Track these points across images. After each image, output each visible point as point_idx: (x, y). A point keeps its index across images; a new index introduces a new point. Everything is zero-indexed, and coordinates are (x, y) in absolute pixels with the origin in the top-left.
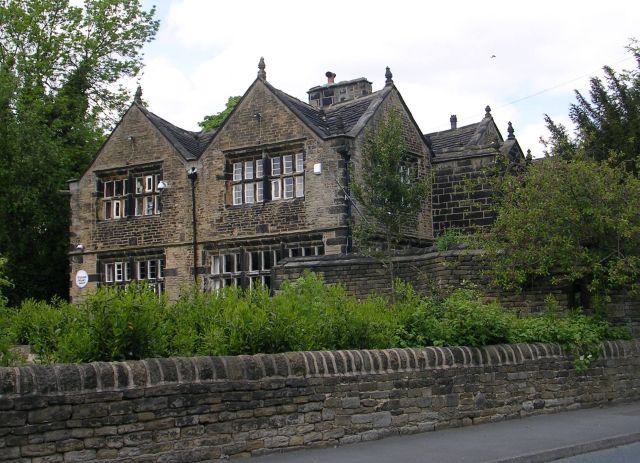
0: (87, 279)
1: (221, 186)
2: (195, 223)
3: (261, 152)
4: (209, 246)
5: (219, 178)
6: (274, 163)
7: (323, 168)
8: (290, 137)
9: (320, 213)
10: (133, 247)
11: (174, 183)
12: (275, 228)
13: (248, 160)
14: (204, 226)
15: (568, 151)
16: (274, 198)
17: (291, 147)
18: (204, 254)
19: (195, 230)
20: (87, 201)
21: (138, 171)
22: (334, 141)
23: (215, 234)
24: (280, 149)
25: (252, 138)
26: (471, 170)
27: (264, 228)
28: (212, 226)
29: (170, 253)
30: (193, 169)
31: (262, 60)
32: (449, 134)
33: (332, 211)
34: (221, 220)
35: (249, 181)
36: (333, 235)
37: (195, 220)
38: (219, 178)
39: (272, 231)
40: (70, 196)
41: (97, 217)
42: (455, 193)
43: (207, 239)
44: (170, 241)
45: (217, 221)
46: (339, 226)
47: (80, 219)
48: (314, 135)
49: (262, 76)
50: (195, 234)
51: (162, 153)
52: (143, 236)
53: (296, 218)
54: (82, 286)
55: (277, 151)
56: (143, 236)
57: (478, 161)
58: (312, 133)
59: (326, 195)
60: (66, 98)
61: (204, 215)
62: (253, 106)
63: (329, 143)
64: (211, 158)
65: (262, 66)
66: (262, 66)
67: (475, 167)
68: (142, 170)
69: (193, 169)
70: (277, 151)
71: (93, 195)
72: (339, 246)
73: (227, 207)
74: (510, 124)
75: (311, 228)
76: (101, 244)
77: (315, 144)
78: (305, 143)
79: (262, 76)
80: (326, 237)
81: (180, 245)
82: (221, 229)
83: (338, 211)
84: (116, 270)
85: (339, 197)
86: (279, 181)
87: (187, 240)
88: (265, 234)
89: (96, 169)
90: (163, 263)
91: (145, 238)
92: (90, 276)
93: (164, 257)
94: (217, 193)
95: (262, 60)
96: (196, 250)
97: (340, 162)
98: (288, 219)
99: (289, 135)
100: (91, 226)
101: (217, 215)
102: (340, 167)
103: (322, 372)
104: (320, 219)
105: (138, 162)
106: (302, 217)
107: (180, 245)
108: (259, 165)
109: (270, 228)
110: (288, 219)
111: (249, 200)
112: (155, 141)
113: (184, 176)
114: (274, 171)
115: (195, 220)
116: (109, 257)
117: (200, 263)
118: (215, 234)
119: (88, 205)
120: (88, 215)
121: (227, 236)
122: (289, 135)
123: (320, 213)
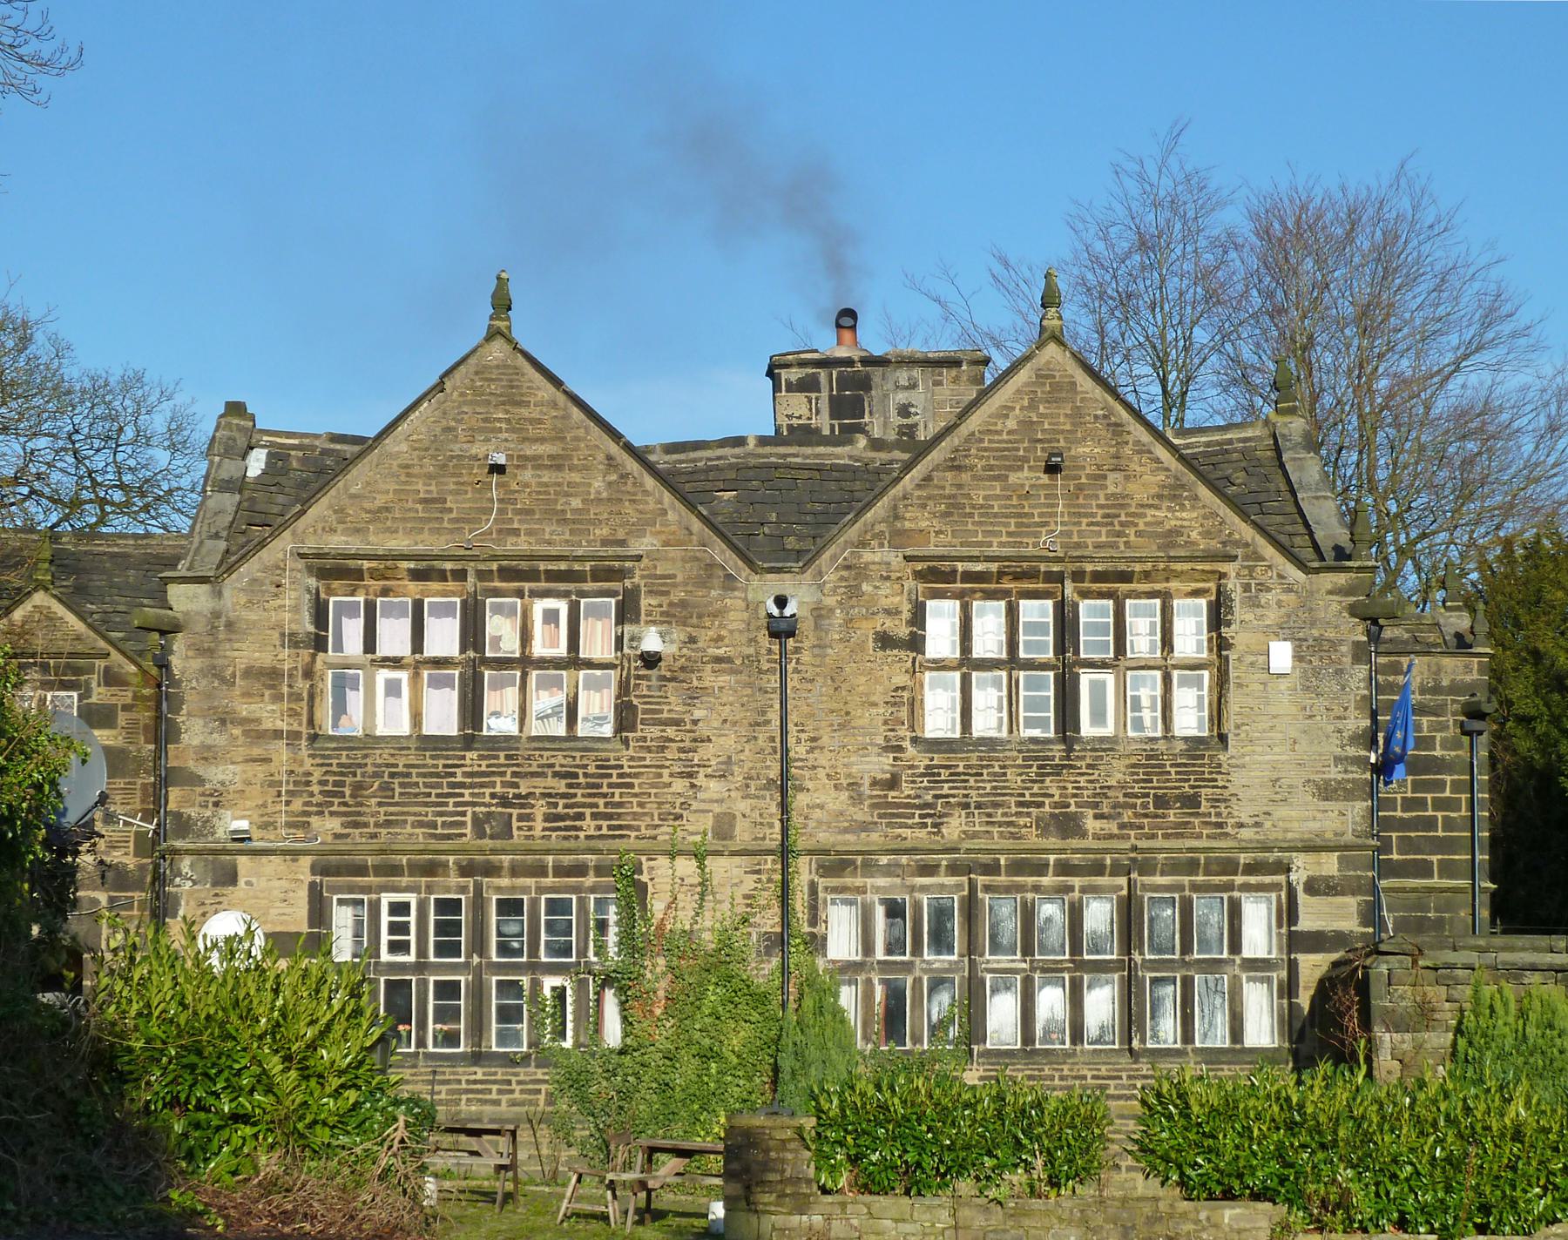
2: (784, 786)
4: (836, 864)
11: (692, 640)
12: (1111, 826)
13: (990, 595)
15: (1490, 557)
18: (813, 888)
19: (784, 807)
21: (507, 574)
23: (865, 827)
25: (1026, 526)
28: (857, 799)
33: (1327, 792)
34: (893, 783)
36: (1330, 865)
37: (785, 775)
40: (136, 855)
43: (824, 838)
46: (1349, 838)
53: (1191, 802)
56: (540, 809)
58: (1261, 541)
60: (85, 1048)
62: (1027, 424)
64: (855, 572)
68: (533, 575)
69: (781, 602)
80: (1303, 868)
82: (890, 812)
83: (1349, 796)
84: (385, 919)
85: (1352, 751)
88: (1075, 843)
89: (311, 545)
91: (548, 818)
97: (1357, 644)
98: (1161, 802)
100: (281, 754)
101: (881, 765)
104: (1281, 812)
105: (522, 545)
108: (1039, 612)
109: (1091, 824)
111: (987, 722)
115: (785, 775)
118: (865, 827)
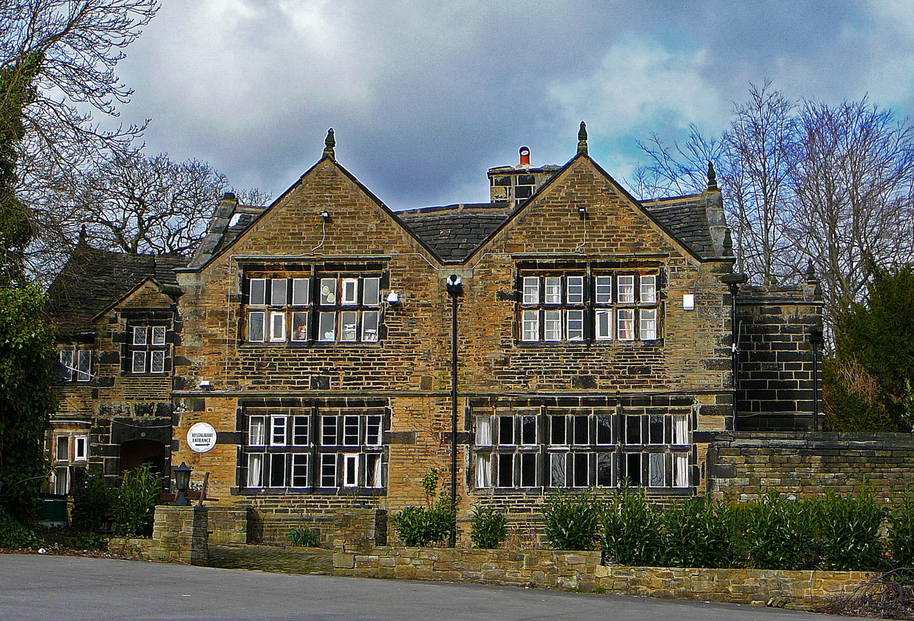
0: (214, 439)
2: (455, 364)
3: (584, 266)
4: (477, 402)
5: (502, 296)
6: (602, 283)
7: (696, 302)
8: (639, 250)
9: (687, 363)
11: (413, 296)
14: (471, 370)
16: (598, 337)
17: (637, 264)
18: (468, 414)
22: (718, 265)
25: (569, 243)
26: (781, 321)
27: (587, 382)
28: (488, 370)
29: (398, 406)
30: (454, 278)
32: (482, 213)
34: (505, 362)
35: (554, 307)
36: (712, 401)
37: (455, 359)
38: (502, 296)
39: (602, 386)
41: (240, 336)
44: (400, 386)
47: (200, 335)
48: (683, 252)
51: (388, 246)
52: (342, 375)
53: (646, 370)
54: (202, 449)
55: (610, 266)
56: (342, 375)
57: (792, 309)
59: (700, 342)
61: (472, 351)
62: (570, 194)
63: (710, 266)
67: (786, 318)
68: (341, 267)
69: (454, 278)
70: (610, 266)
72: (723, 418)
73: (517, 342)
74: (331, 133)
75: (673, 387)
76: (249, 383)
77: (685, 265)
78: (665, 260)
81: (422, 396)
83: (722, 368)
85: (723, 347)
86: (609, 312)
87: (435, 388)
88: (591, 390)
90: (387, 425)
92: (219, 435)
96: (456, 404)
99: (637, 246)
102: (725, 303)
104: (689, 375)
107: (422, 396)
109: (599, 382)
112: (372, 225)
113: (434, 286)
115: (455, 359)
116: (261, 404)
117: (461, 426)
118: (492, 383)
121: (515, 387)
122: (637, 246)
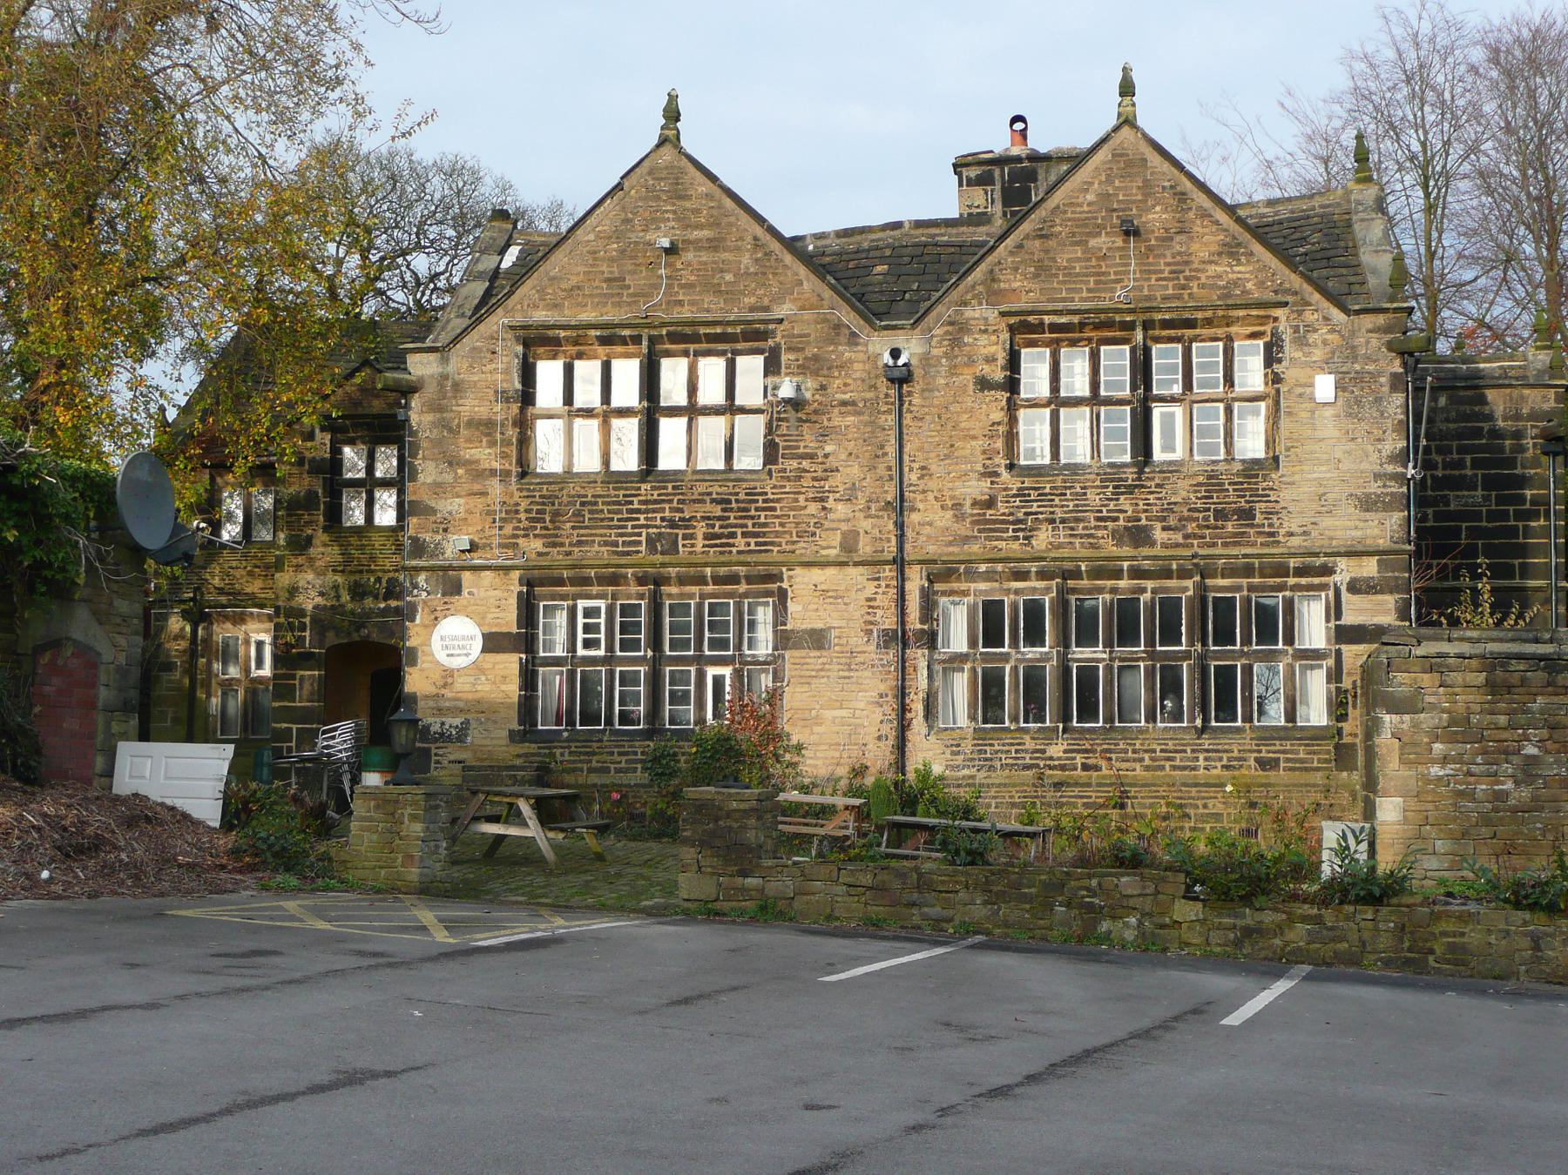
0: (478, 644)
1: (993, 407)
2: (900, 507)
3: (1130, 326)
5: (984, 384)
10: (659, 558)
12: (1179, 538)
20: (483, 412)
22: (1381, 319)
23: (966, 539)
24: (1190, 324)
25: (1103, 284)
28: (960, 517)
31: (672, 99)
33: (1368, 504)
34: (990, 503)
36: (1369, 568)
38: (984, 384)
42: (1439, 473)
44: (803, 549)
45: (975, 503)
49: (669, 139)
50: (901, 538)
53: (1247, 515)
55: (1181, 326)
56: (700, 529)
62: (1105, 197)
64: (959, 329)
65: (672, 114)
66: (672, 114)
68: (695, 338)
69: (895, 354)
71: (505, 397)
79: (669, 139)
80: (1345, 571)
82: (989, 527)
83: (1388, 508)
85: (1390, 468)
89: (519, 319)
91: (707, 537)
93: (782, 596)
94: (978, 427)
95: (672, 99)
96: (902, 578)
97: (1394, 376)
98: (1220, 515)
100: (496, 488)
101: (977, 488)
102: (1394, 388)
103: (436, 755)
105: (686, 313)
106: (1268, 514)
109: (1159, 535)
110: (1220, 515)
114: (1166, 379)
118: (966, 539)
119: (486, 427)
120: (485, 455)
123: (1327, 508)
